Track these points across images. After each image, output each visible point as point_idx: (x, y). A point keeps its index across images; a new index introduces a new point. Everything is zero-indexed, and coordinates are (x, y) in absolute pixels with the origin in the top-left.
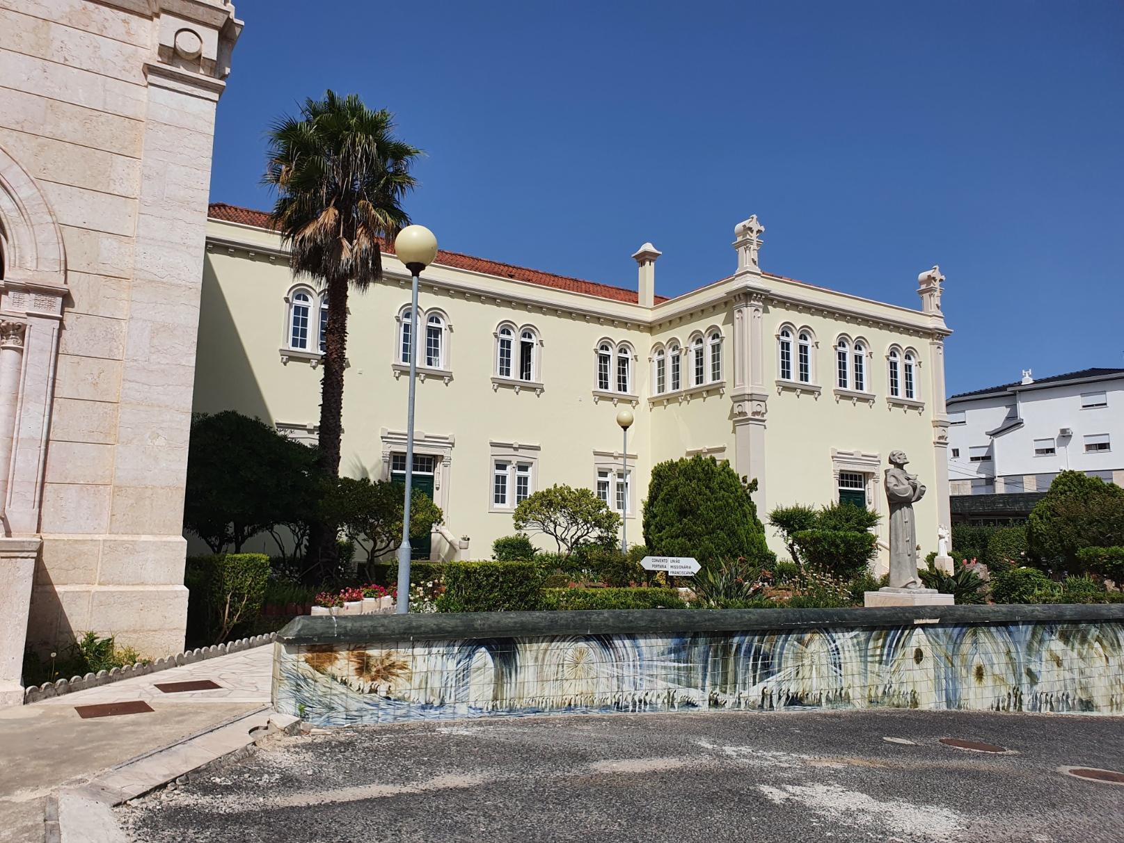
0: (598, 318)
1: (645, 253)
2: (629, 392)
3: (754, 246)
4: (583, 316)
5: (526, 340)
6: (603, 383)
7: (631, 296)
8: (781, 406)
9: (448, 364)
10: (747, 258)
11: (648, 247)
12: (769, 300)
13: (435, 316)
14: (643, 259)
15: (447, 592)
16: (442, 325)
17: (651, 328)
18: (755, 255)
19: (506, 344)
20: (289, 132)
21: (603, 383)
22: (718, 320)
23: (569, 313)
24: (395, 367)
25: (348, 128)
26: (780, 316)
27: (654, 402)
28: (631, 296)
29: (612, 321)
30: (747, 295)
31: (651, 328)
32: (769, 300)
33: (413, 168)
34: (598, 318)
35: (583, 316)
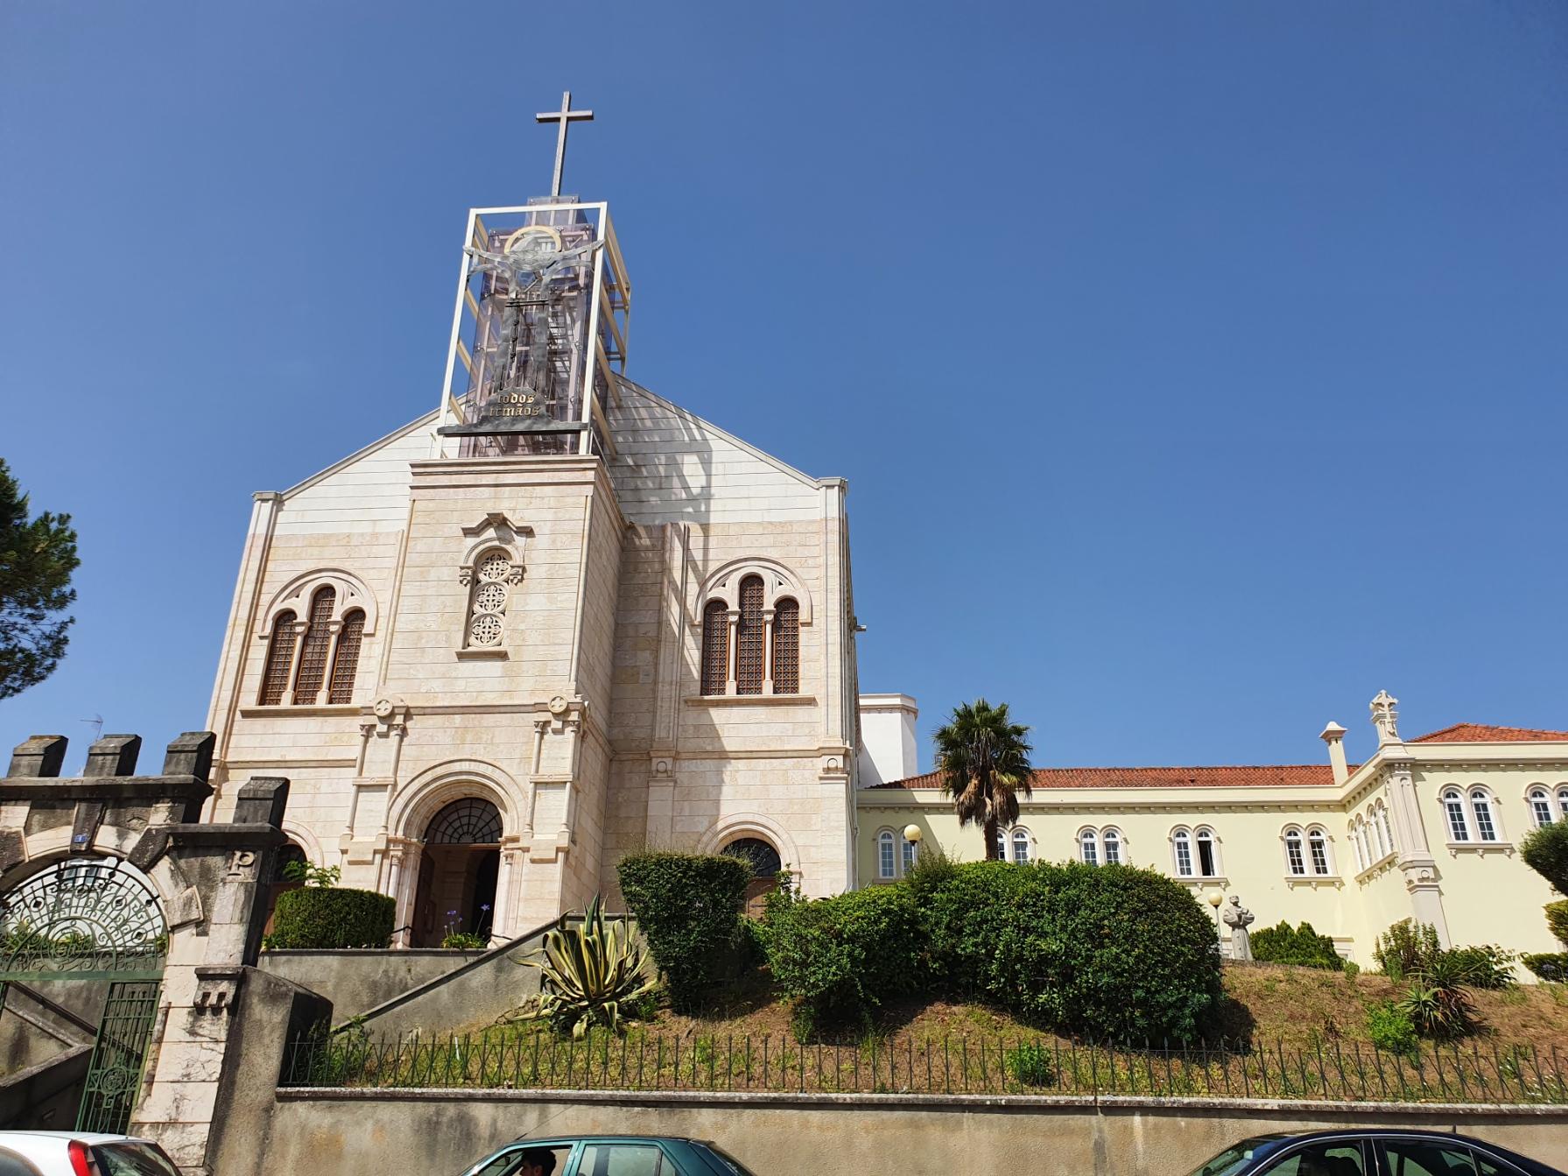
0: (1278, 807)
1: (1328, 733)
2: (1330, 873)
3: (1388, 719)
4: (1262, 807)
5: (1203, 839)
6: (1297, 866)
7: (1323, 775)
8: (1456, 870)
9: (1505, 836)
10: (1384, 731)
11: (1333, 726)
12: (1416, 768)
13: (1110, 832)
14: (1330, 737)
15: (1020, 994)
16: (1118, 839)
17: (1343, 806)
18: (1389, 727)
19: (1183, 847)
20: (944, 734)
21: (1297, 866)
22: (1379, 793)
23: (1229, 807)
24: (1450, 846)
25: (976, 726)
26: (1435, 782)
27: (1365, 878)
28: (1323, 775)
29: (1296, 806)
30: (1390, 766)
31: (1343, 806)
32: (1416, 768)
33: (1028, 739)
34: (1278, 807)
35: (1262, 807)
